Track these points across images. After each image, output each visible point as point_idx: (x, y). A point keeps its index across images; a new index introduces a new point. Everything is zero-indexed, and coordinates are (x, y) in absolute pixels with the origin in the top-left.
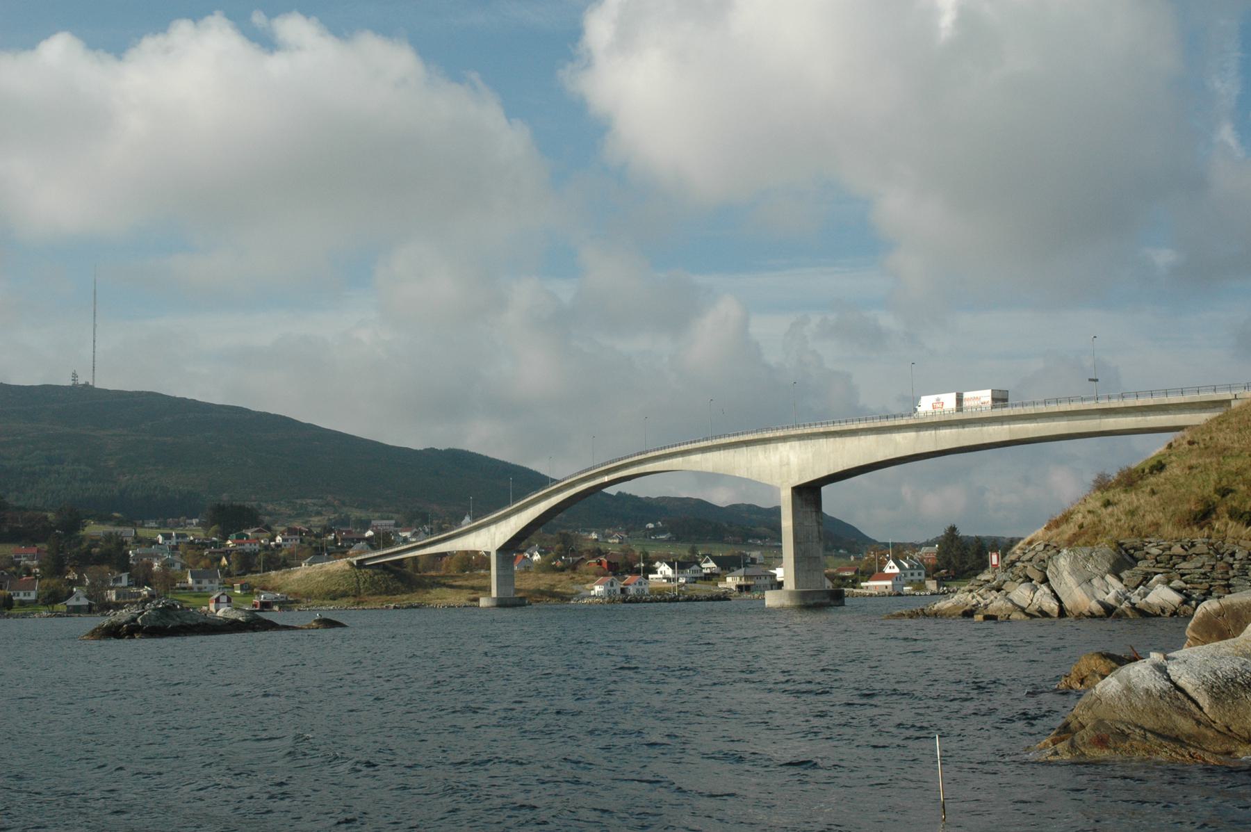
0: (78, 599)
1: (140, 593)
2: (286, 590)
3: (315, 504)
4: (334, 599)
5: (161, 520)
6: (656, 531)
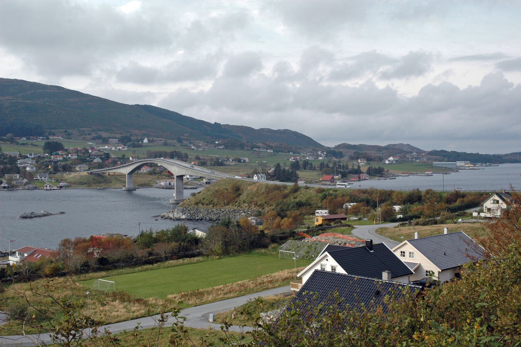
0: (4, 184)
1: (23, 182)
2: (68, 181)
3: (88, 130)
4: (82, 185)
5: (28, 137)
6: (219, 145)
